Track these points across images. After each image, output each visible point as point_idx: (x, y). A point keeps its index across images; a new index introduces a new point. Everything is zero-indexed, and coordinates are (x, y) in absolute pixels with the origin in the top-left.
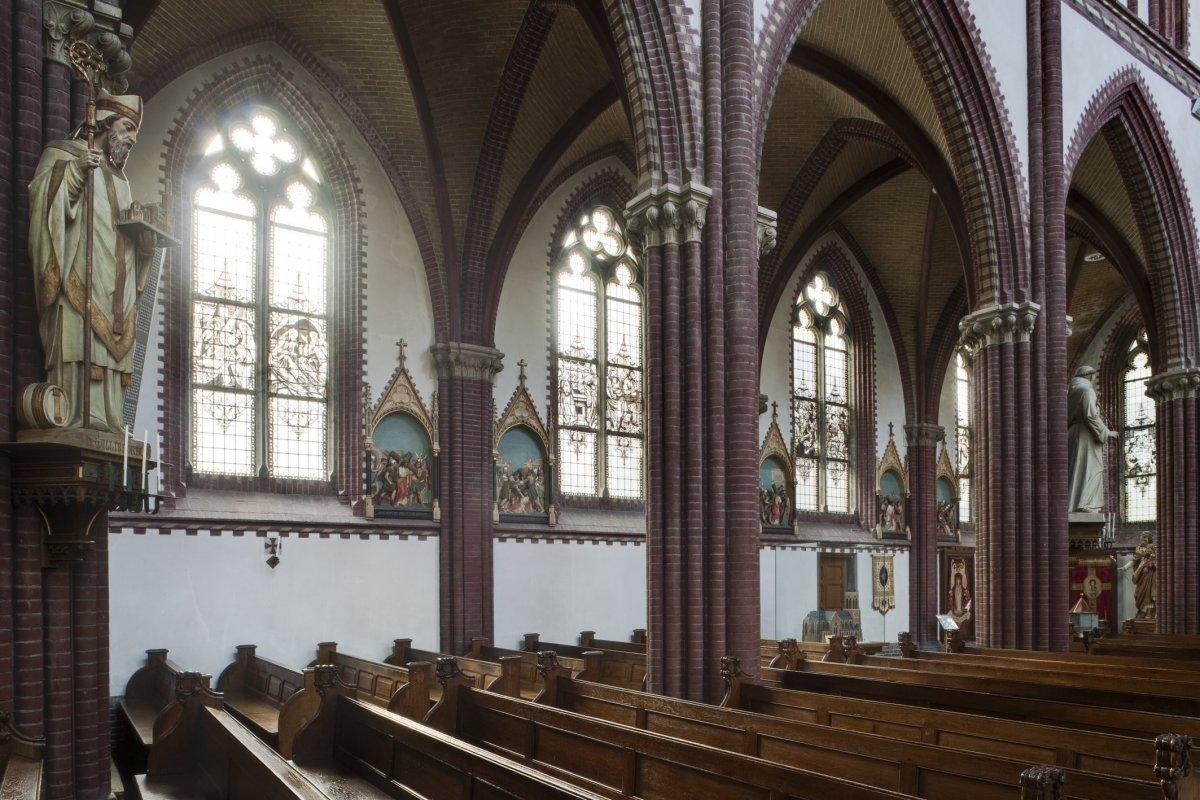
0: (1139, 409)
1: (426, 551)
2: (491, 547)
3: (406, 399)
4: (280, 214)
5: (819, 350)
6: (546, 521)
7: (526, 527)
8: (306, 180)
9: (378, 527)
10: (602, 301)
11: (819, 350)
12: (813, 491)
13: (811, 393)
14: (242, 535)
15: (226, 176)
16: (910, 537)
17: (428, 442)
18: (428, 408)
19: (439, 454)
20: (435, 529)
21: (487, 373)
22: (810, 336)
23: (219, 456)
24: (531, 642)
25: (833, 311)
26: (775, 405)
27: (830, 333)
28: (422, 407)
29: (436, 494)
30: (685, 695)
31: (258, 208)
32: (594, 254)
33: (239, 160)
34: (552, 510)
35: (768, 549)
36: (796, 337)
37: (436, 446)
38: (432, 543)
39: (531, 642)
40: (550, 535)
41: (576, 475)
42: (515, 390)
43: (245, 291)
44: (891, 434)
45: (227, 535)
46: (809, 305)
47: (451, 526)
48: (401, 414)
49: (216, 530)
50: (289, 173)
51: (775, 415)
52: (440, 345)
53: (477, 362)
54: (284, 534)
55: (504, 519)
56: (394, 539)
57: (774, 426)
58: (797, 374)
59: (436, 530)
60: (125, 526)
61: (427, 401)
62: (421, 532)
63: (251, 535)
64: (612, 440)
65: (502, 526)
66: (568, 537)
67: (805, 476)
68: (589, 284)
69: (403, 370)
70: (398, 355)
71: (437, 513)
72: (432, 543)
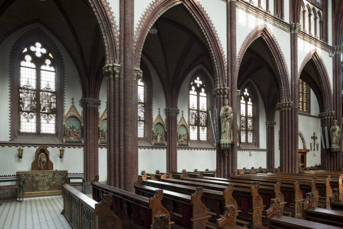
0: (27, 80)
1: (163, 153)
2: (177, 150)
3: (160, 121)
4: (201, 94)
5: (246, 105)
6: (188, 145)
7: (184, 147)
8: (49, 58)
9: (67, 145)
10: (198, 96)
11: (246, 105)
12: (245, 137)
13: (245, 115)
14: (4, 147)
15: (28, 58)
16: (215, 146)
17: (81, 123)
18: (80, 115)
19: (83, 126)
20: (83, 146)
21: (96, 105)
22: (244, 102)
23: (47, 129)
24: (184, 171)
25: (202, 86)
26: (183, 112)
27: (249, 101)
28: (79, 115)
29: (166, 140)
30: (120, 188)
31: (197, 93)
32: (245, 96)
33: (32, 54)
34: (241, 145)
35: (239, 151)
36: (241, 102)
37: (83, 125)
38: (82, 149)
39: (184, 171)
40: (188, 148)
41: (193, 136)
42: (157, 115)
43: (196, 108)
44: (159, 112)
45: (6, 147)
46: (195, 85)
47: (86, 145)
48: (73, 117)
49: (29, 146)
50: (45, 57)
51: (183, 115)
52: (84, 99)
53: (93, 103)
54: (24, 147)
55: (179, 145)
56: (72, 148)
57: (183, 118)
58: (241, 111)
59: (83, 146)
60: (49, 146)
61: (164, 121)
62: (163, 148)
63: (56, 148)
64: (201, 128)
65: (179, 147)
66: (145, 148)
67: (250, 135)
68: (196, 93)
69: (73, 106)
70: (160, 110)
71: (166, 144)
72: (82, 149)
